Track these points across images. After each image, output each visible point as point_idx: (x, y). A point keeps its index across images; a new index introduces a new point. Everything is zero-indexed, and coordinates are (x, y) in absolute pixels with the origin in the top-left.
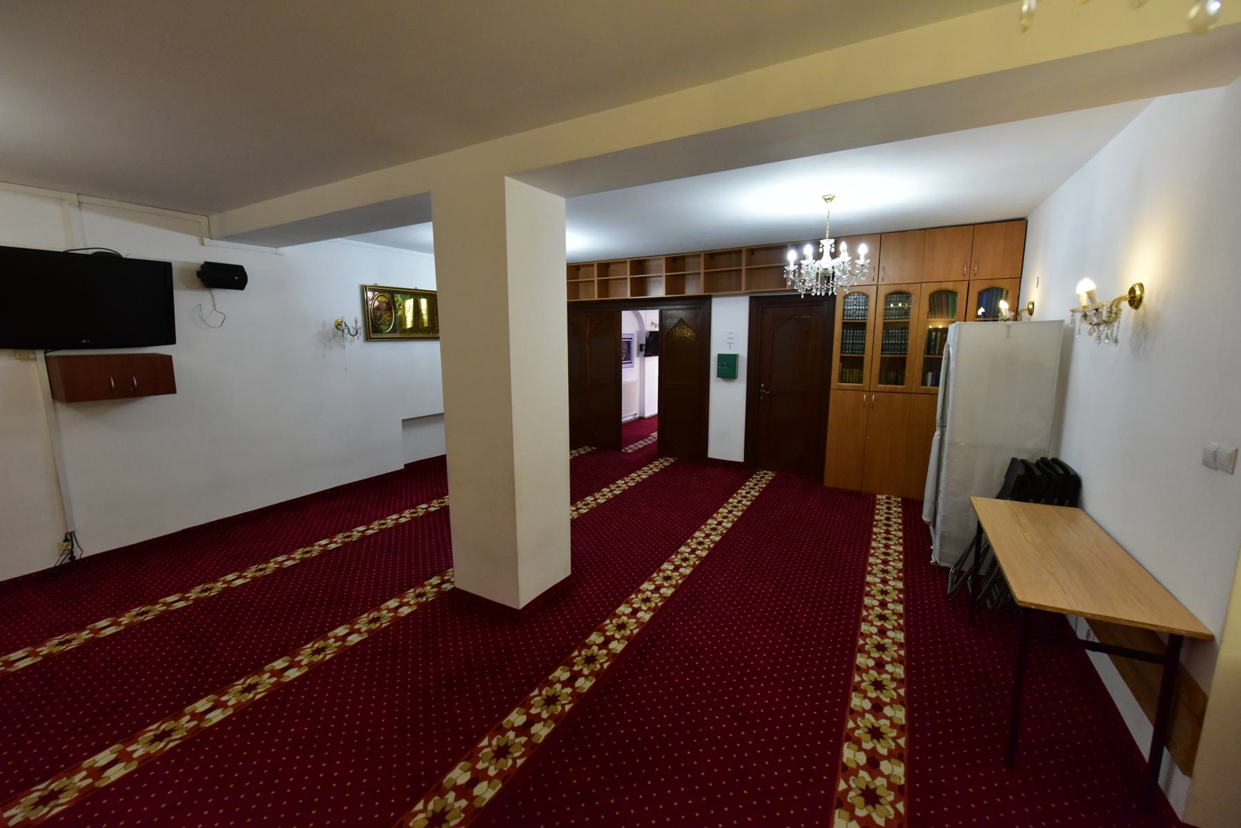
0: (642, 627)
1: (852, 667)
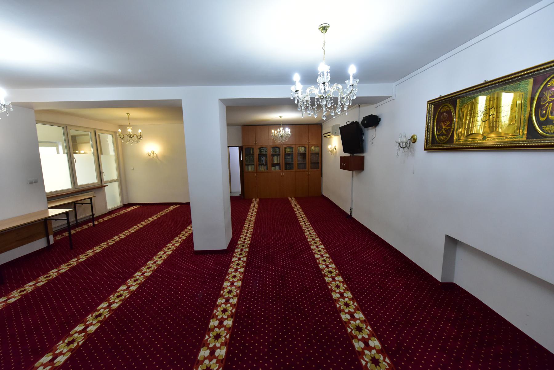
0: (230, 331)
1: (311, 250)
